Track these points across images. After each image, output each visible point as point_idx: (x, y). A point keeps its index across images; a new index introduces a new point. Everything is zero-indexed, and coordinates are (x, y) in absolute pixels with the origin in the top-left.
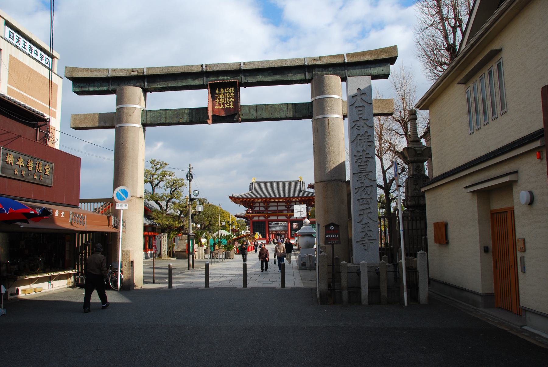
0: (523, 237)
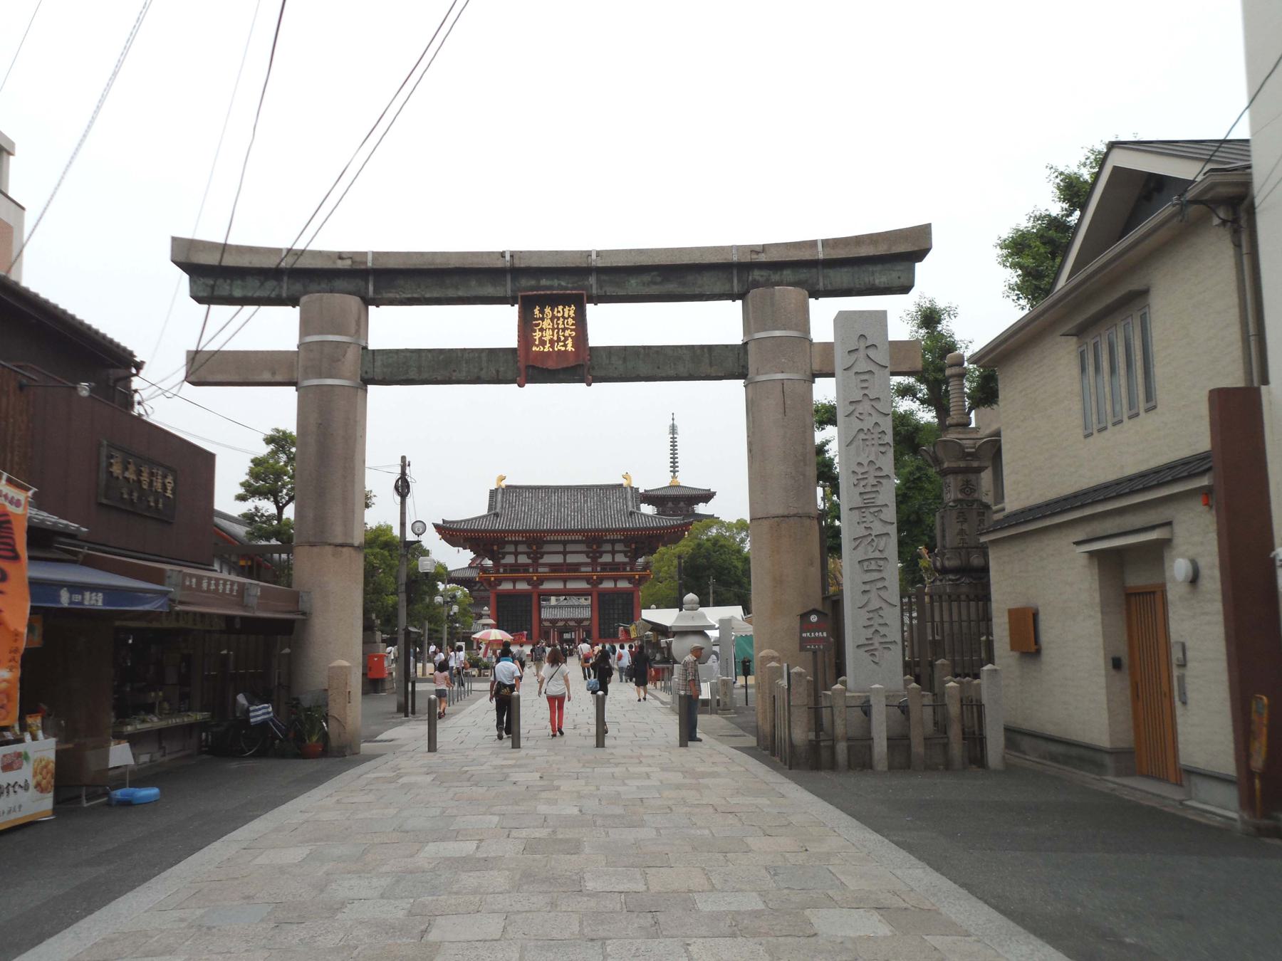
0: (1182, 640)
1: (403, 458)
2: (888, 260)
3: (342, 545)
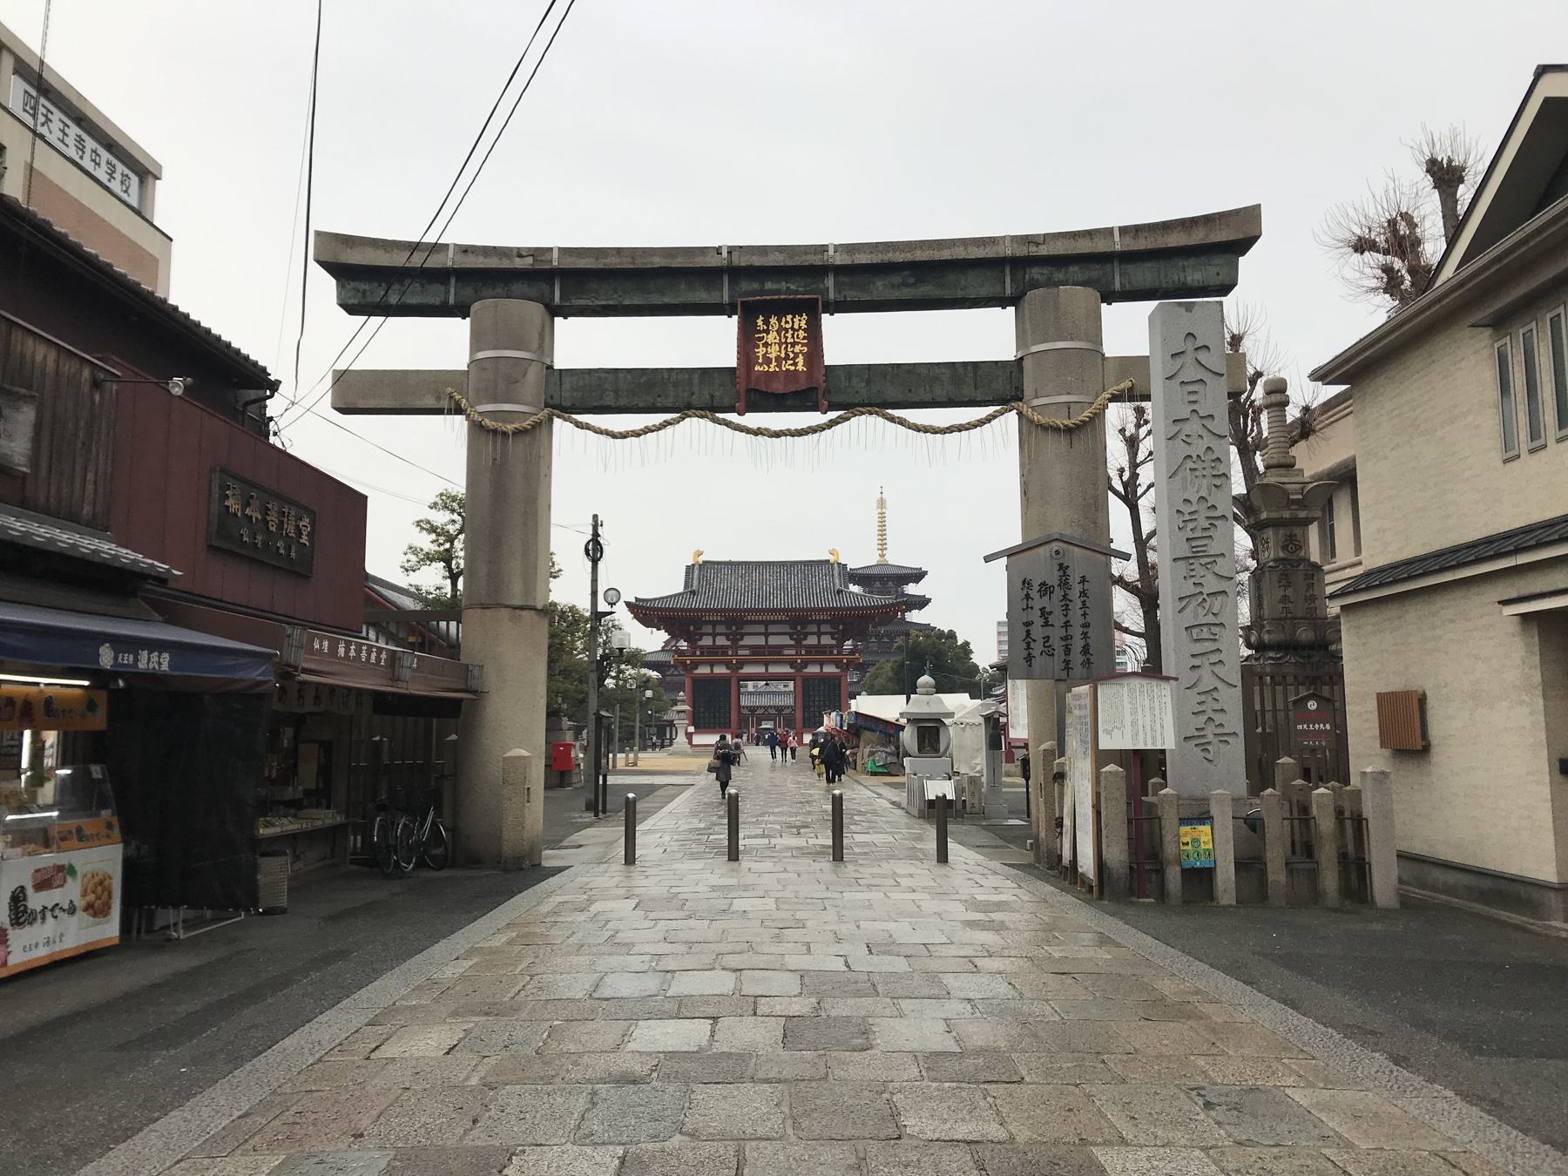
1: (595, 517)
2: (1194, 259)
3: (522, 608)
